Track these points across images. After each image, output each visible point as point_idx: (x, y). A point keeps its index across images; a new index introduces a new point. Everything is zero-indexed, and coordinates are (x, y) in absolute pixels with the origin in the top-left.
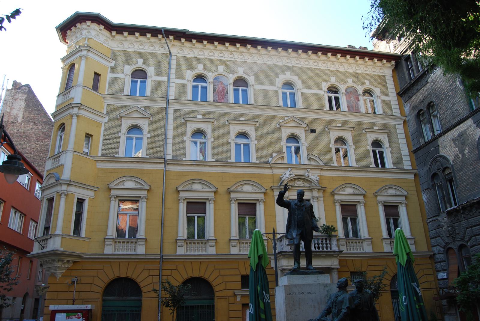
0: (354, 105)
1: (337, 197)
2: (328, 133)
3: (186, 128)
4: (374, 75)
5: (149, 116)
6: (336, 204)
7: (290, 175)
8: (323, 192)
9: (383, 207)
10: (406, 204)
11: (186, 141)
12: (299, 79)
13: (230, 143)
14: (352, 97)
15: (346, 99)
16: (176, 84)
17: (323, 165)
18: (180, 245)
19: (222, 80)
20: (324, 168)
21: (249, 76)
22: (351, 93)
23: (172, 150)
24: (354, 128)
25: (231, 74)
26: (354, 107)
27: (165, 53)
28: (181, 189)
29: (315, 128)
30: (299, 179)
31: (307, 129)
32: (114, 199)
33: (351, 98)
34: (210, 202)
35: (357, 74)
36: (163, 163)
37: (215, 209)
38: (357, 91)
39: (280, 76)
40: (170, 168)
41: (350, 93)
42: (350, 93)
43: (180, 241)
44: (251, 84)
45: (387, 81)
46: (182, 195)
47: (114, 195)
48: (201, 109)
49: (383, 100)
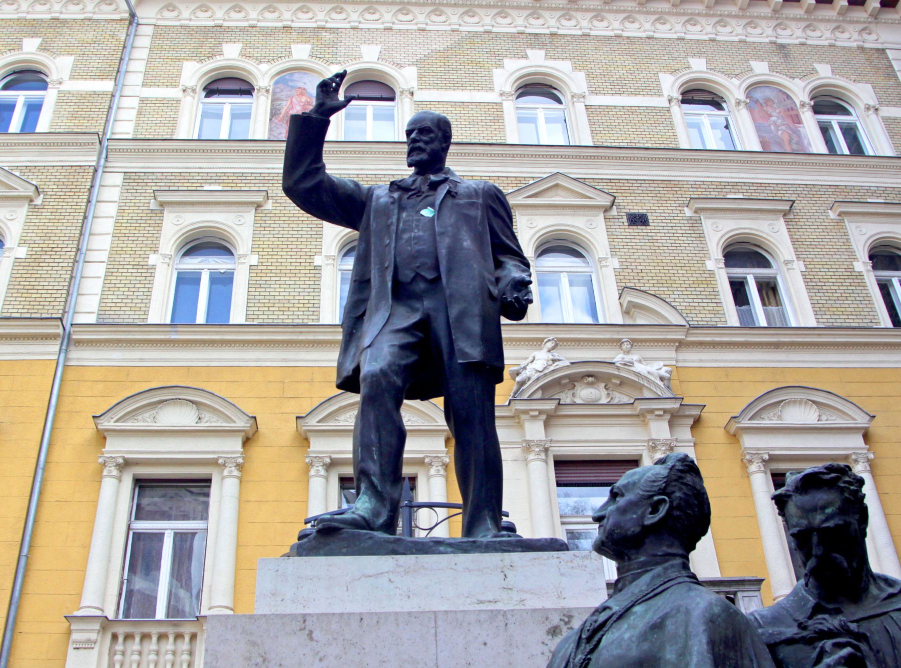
0: (786, 137)
1: (749, 442)
2: (695, 223)
3: (159, 226)
4: (844, 48)
5: (30, 192)
6: (753, 468)
7: (550, 362)
8: (692, 427)
9: (767, 478)
10: (868, 460)
11: (154, 267)
12: (575, 69)
13: (318, 268)
14: (774, 114)
15: (754, 120)
16: (143, 101)
17: (684, 323)
18: (80, 642)
19: (305, 84)
20: (691, 339)
21: (399, 66)
22: (769, 104)
23: (101, 299)
24: (794, 202)
25: (336, 63)
26: (787, 143)
27: (117, 17)
28: (112, 423)
29: (644, 211)
30: (590, 379)
31: (614, 212)
32: (115, 472)
33: (770, 116)
34: (226, 473)
35: (782, 47)
36: (54, 337)
37: (242, 501)
38: (788, 97)
39: (506, 61)
40: (79, 356)
41: (766, 103)
42: (766, 103)
43: (82, 626)
44: (404, 86)
45: (893, 62)
46: (117, 447)
47: (233, 456)
48: (494, 172)
49: (890, 118)
